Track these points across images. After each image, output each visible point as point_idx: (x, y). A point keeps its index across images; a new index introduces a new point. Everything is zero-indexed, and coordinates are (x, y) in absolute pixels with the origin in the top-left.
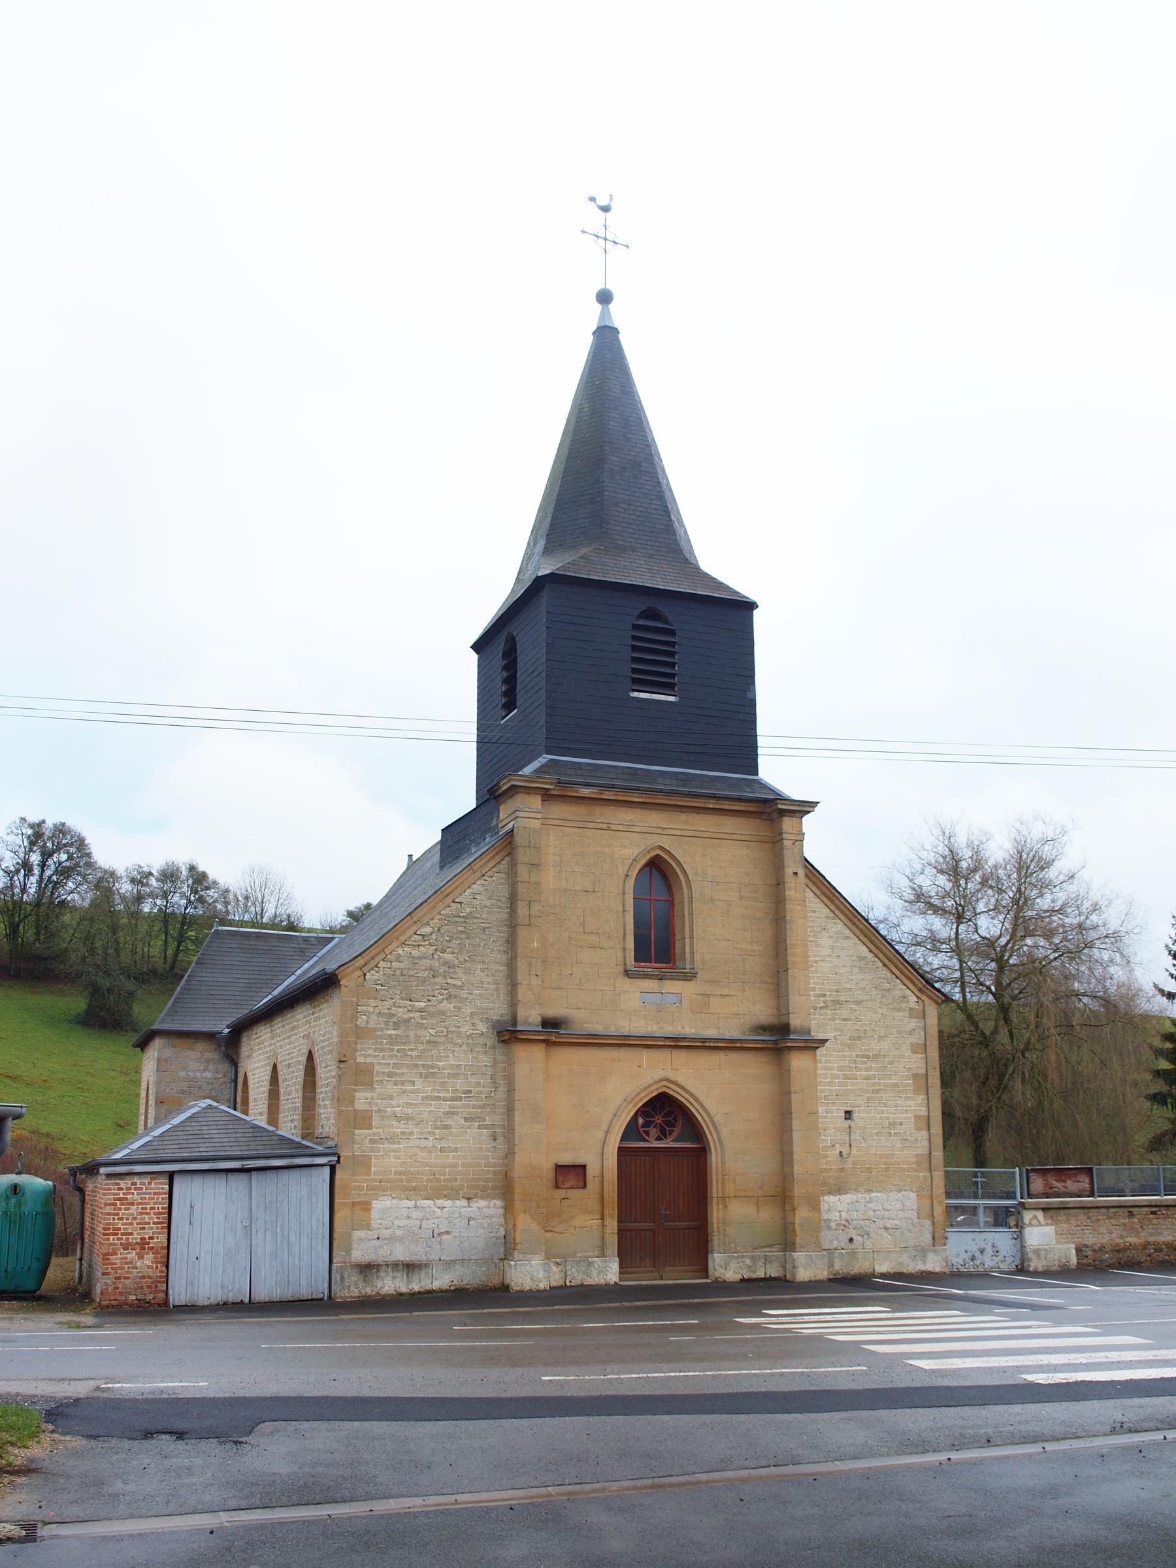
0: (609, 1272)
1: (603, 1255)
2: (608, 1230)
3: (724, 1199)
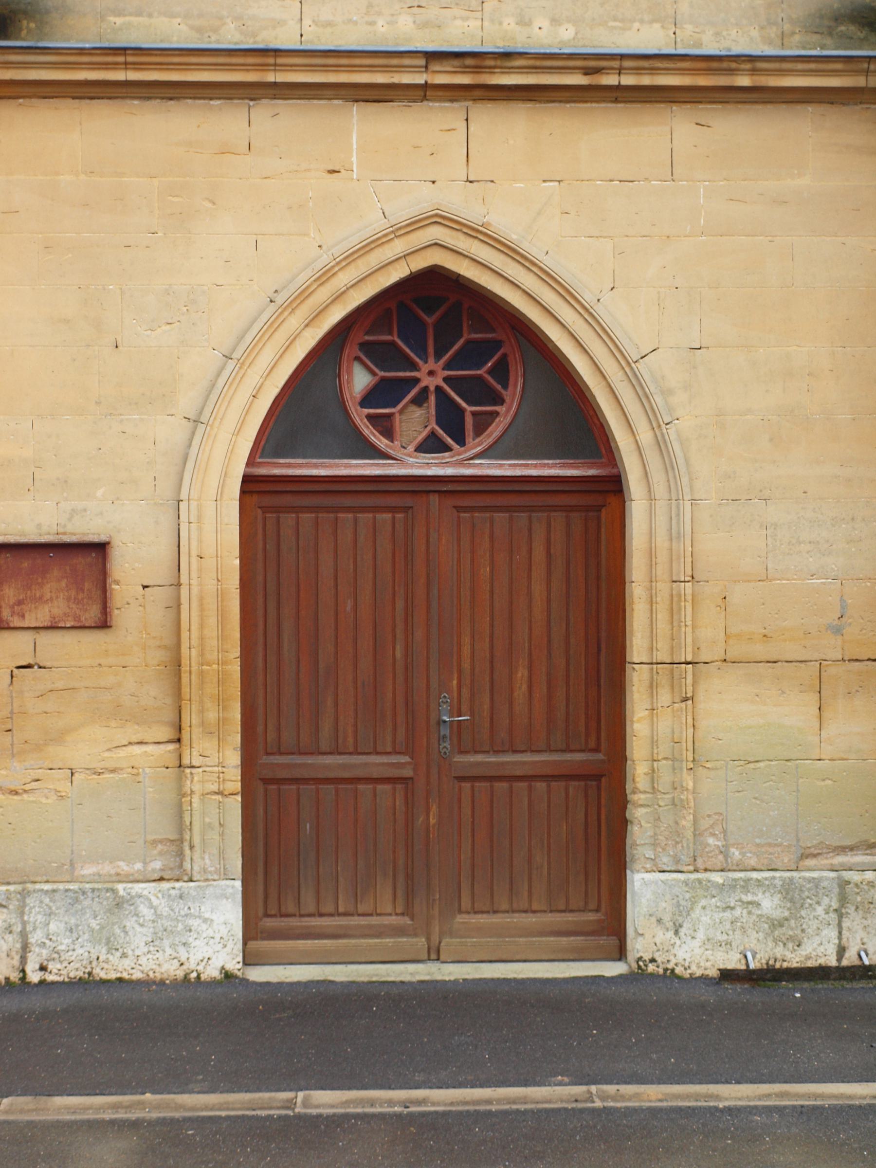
0: (199, 931)
1: (177, 872)
2: (198, 783)
3: (683, 669)
